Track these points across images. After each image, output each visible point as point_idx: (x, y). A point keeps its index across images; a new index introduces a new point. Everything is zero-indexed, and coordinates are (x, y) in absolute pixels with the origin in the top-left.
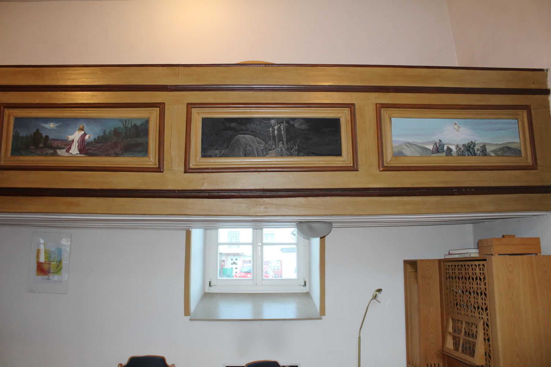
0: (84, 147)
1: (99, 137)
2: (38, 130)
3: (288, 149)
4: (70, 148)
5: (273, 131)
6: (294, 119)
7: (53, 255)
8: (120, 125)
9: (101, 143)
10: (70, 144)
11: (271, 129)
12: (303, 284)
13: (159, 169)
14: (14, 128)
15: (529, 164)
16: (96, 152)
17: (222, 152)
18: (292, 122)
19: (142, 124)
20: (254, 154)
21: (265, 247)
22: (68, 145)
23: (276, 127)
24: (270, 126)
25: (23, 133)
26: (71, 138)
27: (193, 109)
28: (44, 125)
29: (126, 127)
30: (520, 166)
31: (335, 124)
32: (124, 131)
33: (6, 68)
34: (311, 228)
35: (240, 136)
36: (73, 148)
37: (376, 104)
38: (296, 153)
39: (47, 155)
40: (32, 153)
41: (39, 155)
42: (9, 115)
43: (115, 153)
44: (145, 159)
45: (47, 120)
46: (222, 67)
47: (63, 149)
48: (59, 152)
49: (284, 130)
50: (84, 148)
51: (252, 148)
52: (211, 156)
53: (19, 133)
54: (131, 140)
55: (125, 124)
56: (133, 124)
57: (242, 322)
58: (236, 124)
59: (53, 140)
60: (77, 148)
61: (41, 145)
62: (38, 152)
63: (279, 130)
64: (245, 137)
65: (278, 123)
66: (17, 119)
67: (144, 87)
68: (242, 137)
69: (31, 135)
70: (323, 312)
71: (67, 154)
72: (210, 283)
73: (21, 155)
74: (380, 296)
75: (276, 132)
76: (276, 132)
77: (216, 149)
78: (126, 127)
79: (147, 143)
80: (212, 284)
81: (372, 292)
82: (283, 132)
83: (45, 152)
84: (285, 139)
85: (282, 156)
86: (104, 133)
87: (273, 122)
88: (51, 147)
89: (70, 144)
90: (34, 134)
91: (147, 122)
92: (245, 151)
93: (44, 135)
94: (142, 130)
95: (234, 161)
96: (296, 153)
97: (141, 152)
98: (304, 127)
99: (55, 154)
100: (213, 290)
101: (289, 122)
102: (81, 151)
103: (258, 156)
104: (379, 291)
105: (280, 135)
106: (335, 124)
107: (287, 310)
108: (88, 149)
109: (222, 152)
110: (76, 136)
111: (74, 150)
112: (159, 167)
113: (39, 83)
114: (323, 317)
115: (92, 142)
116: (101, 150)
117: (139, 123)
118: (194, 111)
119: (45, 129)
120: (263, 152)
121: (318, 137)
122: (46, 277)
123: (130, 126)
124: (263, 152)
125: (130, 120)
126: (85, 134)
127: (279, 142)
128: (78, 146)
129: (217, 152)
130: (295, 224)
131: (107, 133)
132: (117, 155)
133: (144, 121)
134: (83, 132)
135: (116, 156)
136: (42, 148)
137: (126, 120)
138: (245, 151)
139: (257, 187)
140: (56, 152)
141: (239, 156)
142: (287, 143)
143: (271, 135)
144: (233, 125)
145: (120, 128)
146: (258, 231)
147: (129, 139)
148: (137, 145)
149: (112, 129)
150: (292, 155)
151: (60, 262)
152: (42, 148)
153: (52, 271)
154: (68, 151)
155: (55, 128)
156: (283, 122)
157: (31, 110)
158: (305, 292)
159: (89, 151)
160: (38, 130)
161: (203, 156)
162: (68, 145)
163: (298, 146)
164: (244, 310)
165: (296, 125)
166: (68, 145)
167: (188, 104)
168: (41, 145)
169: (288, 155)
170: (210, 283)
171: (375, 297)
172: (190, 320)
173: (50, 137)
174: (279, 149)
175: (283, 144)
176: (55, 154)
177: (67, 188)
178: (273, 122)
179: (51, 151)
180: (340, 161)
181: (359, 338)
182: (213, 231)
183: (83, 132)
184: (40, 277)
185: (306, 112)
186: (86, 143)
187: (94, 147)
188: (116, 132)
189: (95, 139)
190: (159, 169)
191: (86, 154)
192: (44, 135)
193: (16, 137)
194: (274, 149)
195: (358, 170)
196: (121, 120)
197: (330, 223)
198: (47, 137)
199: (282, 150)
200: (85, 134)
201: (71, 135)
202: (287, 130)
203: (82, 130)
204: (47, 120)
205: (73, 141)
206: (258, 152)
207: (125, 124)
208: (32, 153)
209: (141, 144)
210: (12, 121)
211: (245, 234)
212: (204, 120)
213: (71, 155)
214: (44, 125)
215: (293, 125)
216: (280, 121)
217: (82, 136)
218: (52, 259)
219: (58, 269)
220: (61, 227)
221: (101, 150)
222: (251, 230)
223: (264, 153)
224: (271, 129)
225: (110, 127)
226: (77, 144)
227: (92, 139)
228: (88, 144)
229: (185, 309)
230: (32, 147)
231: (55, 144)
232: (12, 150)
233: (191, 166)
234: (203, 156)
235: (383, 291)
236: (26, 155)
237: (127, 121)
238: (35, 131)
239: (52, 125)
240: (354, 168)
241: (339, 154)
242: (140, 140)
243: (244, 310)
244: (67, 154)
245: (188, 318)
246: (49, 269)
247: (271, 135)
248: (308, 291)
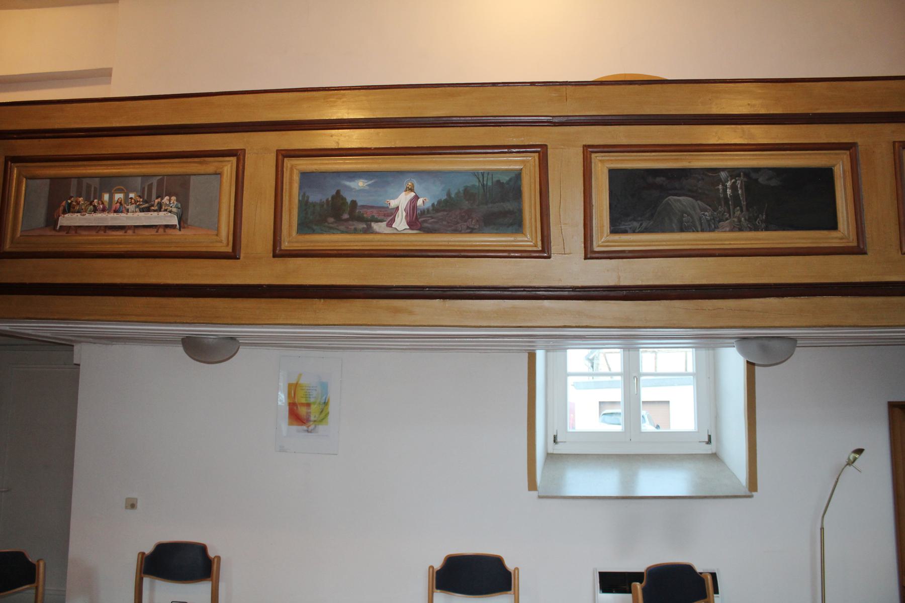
0: (417, 218)
1: (439, 202)
2: (338, 192)
3: (749, 220)
4: (393, 220)
5: (725, 190)
6: (757, 170)
7: (314, 393)
8: (474, 182)
9: (444, 210)
10: (392, 214)
11: (720, 187)
12: (707, 440)
13: (545, 251)
14: (300, 188)
15: (851, 244)
16: (437, 226)
17: (644, 225)
18: (754, 176)
19: (510, 180)
20: (695, 227)
21: (642, 378)
22: (388, 215)
23: (729, 184)
24: (720, 181)
25: (315, 197)
26: (393, 203)
27: (593, 155)
28: (348, 183)
29: (483, 185)
30: (830, 247)
31: (825, 176)
32: (481, 191)
33: (291, 94)
34: (764, 349)
35: (672, 198)
36: (398, 220)
37: (894, 142)
38: (763, 225)
39: (356, 231)
40: (331, 228)
41: (343, 232)
42: (292, 169)
43: (468, 228)
44: (520, 238)
45: (353, 175)
46: (637, 86)
47: (381, 221)
48: (376, 226)
49: (741, 188)
50: (416, 220)
51: (692, 217)
52: (625, 232)
53: (308, 197)
54: (494, 206)
55: (481, 179)
56: (495, 179)
57: (623, 501)
58: (663, 179)
59: (363, 206)
60: (404, 220)
61: (346, 216)
62: (342, 228)
63: (734, 187)
64: (679, 200)
65: (732, 177)
66: (304, 175)
67: (426, 118)
68: (675, 200)
69: (327, 200)
70: (753, 484)
71: (388, 230)
72: (555, 438)
73: (314, 232)
74: (861, 458)
75: (729, 192)
76: (729, 192)
77: (634, 220)
78: (483, 185)
79: (521, 211)
80: (558, 440)
81: (848, 454)
82: (740, 192)
83: (353, 227)
84: (744, 203)
85: (741, 230)
86: (449, 194)
87: (723, 175)
88: (361, 219)
89: (392, 214)
90: (333, 197)
91: (518, 175)
92: (681, 222)
93: (349, 200)
94: (510, 188)
95: (468, 239)
96: (763, 225)
97: (512, 224)
98: (774, 183)
99: (368, 230)
100: (560, 449)
101: (749, 174)
102: (412, 224)
103: (703, 231)
104: (859, 451)
105: (735, 196)
106: (825, 176)
107: (669, 482)
108: (425, 221)
109: (644, 225)
110: (402, 200)
111: (401, 223)
112: (543, 251)
113: (715, 110)
114: (754, 493)
115: (428, 210)
116: (445, 223)
117: (505, 179)
118: (596, 158)
119: (349, 189)
120: (709, 225)
121: (794, 198)
122: (305, 427)
123: (490, 184)
124: (709, 225)
125: (490, 173)
126: (416, 198)
127: (735, 207)
128: (406, 216)
129: (636, 224)
130: (733, 341)
131: (453, 196)
132: (472, 231)
133: (513, 175)
134: (413, 194)
135: (471, 232)
136: (347, 220)
137: (483, 174)
138: (681, 222)
139: (600, 284)
140: (370, 227)
141: (672, 231)
142: (747, 210)
143: (722, 196)
144: (659, 180)
145: (474, 186)
146: (632, 353)
147: (490, 205)
148: (505, 214)
149: (461, 189)
150: (756, 229)
151: (326, 403)
152: (347, 220)
153: (312, 418)
154: (390, 225)
155: (367, 188)
156: (739, 176)
157: (325, 160)
158: (710, 452)
159: (426, 225)
160: (338, 192)
161: (614, 231)
162: (389, 215)
163: (767, 215)
164: (604, 482)
165: (760, 180)
166: (389, 215)
167: (586, 147)
168: (346, 216)
169: (751, 230)
170: (555, 438)
171: (850, 463)
172: (540, 497)
173: (359, 204)
174: (736, 220)
175: (742, 211)
176: (368, 230)
177: (395, 284)
178: (723, 175)
179: (362, 226)
180: (836, 238)
181: (822, 529)
182: (559, 354)
183: (413, 194)
184: (295, 428)
185: (653, 160)
186: (419, 212)
187: (432, 218)
188: (468, 193)
189: (433, 205)
190: (545, 251)
191: (419, 230)
192: (349, 200)
193: (304, 205)
194: (727, 219)
195: (865, 253)
196: (475, 174)
197: (793, 340)
198: (354, 203)
199: (740, 221)
200: (416, 198)
201: (393, 199)
202: (747, 188)
203: (412, 190)
204: (353, 175)
205: (397, 208)
206: (701, 225)
207: (481, 179)
208: (330, 230)
209: (511, 213)
210: (296, 178)
211: (612, 358)
212: (613, 173)
213: (395, 232)
214: (348, 183)
215: (756, 180)
216: (734, 172)
217: (411, 200)
218: (312, 400)
219: (323, 415)
220: (313, 347)
221: (445, 223)
222: (690, 353)
223: (711, 226)
224: (720, 187)
225: (457, 186)
226: (404, 214)
227: (428, 205)
228: (423, 213)
229: (529, 481)
230: (331, 220)
231: (368, 214)
232: (299, 225)
233: (855, 244)
234: (614, 231)
235: (864, 453)
236: (322, 232)
237: (485, 175)
238: (334, 193)
239: (361, 184)
240: (859, 250)
241: (834, 226)
242: (509, 206)
243: (604, 482)
244: (388, 230)
245: (534, 494)
246: (308, 414)
247: (722, 196)
248: (714, 451)
